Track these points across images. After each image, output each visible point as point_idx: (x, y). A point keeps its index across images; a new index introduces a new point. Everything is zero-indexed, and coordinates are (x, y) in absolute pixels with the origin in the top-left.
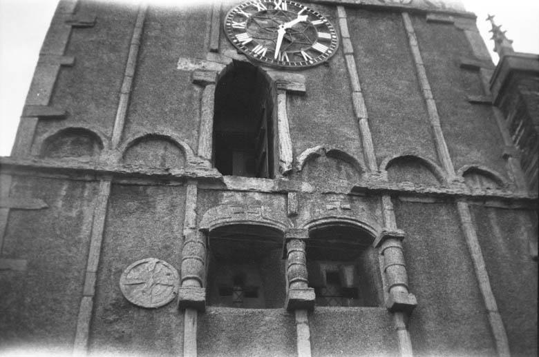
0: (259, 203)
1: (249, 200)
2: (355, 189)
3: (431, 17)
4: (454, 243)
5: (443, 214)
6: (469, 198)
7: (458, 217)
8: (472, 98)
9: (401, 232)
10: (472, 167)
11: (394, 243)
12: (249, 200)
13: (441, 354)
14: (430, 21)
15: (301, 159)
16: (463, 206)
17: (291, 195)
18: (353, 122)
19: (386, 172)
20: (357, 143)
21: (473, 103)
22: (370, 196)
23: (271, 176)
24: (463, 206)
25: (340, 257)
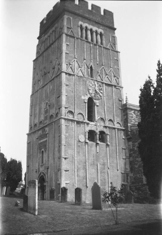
0: (93, 127)
1: (92, 126)
2: (104, 126)
3: (117, 87)
4: (114, 135)
5: (114, 130)
6: (117, 128)
7: (115, 131)
8: (120, 108)
9: (109, 134)
10: (100, 142)
11: (108, 135)
12: (92, 126)
13: (46, 185)
14: (117, 88)
15: (98, 119)
16: (116, 129)
17: (97, 126)
18: (104, 112)
19: (63, 185)
20: (104, 116)
21: (120, 109)
22: (106, 127)
23: (94, 122)
24: (116, 129)
25: (103, 136)
